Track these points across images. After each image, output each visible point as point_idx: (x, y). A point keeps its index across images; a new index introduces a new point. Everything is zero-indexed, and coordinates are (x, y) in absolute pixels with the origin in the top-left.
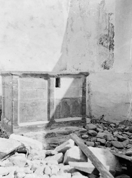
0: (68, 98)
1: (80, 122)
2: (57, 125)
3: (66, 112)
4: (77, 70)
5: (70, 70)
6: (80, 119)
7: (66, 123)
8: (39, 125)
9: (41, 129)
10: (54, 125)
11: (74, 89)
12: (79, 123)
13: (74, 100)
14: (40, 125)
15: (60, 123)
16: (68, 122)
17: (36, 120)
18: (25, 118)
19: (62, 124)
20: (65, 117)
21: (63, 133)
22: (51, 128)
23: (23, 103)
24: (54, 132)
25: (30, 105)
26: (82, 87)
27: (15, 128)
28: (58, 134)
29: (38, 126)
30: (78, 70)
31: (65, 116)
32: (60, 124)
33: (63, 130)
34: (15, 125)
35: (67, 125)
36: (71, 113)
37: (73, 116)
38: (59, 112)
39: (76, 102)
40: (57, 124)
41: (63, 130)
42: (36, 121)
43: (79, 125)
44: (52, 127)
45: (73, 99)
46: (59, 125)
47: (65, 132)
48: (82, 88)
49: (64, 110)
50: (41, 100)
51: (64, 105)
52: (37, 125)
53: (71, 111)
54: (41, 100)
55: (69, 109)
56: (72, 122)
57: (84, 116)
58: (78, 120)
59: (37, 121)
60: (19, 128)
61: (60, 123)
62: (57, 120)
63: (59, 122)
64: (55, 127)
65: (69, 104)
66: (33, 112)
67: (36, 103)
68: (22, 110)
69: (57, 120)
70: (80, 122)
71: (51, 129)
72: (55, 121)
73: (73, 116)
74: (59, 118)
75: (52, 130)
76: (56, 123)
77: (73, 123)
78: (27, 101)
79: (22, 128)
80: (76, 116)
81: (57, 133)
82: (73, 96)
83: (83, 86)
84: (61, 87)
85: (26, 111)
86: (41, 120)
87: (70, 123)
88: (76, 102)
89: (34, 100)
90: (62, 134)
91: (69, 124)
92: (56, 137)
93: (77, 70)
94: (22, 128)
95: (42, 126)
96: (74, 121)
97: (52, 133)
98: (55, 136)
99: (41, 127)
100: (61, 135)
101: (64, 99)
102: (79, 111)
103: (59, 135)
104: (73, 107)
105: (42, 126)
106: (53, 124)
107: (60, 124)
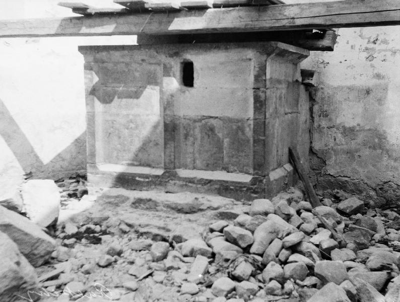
0: (217, 117)
1: (245, 189)
2: (182, 186)
3: (212, 155)
4: (374, 42)
5: (348, 43)
6: (246, 179)
7: (205, 184)
8: (141, 176)
9: (144, 186)
10: (175, 184)
11: (233, 92)
12: (241, 191)
13: (235, 127)
14: (143, 178)
15: (190, 182)
16: (210, 181)
17: (138, 163)
18: (115, 154)
19: (194, 185)
20: (208, 167)
21: (174, 206)
22: (167, 190)
23: (110, 118)
24: (153, 199)
25: (124, 125)
26: (254, 89)
27: (92, 173)
28: (164, 207)
29: (137, 179)
30: (378, 42)
31: (208, 165)
32: (190, 184)
33: (183, 198)
34: (91, 166)
35: (209, 190)
36: (226, 160)
37: (231, 168)
38: (193, 153)
39: (240, 133)
40: (181, 183)
41: (183, 198)
42: (137, 166)
43: (242, 198)
44: (170, 188)
45: (230, 120)
46: (186, 185)
47: (180, 204)
48: (252, 91)
49: (206, 148)
50: (148, 115)
51: (206, 137)
52: (135, 174)
53: (225, 152)
54: (148, 115)
55: (220, 148)
56: (221, 185)
57: (257, 174)
58: (239, 183)
59: (140, 165)
60: (97, 174)
61: (191, 181)
62: (183, 173)
63: (186, 178)
64: (175, 188)
65: (220, 135)
66: (131, 142)
67: (136, 122)
68: (108, 134)
69: (183, 173)
70: (245, 189)
71: (167, 192)
72: (176, 174)
73: (231, 168)
74: (191, 166)
75: (168, 194)
76: (180, 179)
77: (224, 189)
78: (118, 115)
79: (388, 206)
80: (241, 172)
81: (162, 202)
82: (230, 113)
83: (255, 84)
84: (195, 85)
85: (116, 138)
86: (149, 166)
87: (217, 186)
88: (240, 133)
89: (133, 115)
90: (173, 209)
91: (213, 187)
92: (157, 211)
93: (374, 42)
94: (104, 174)
95: (147, 180)
96: (227, 182)
97: (150, 200)
98: (155, 208)
99: (144, 182)
100: (169, 210)
101: (206, 120)
102: (247, 156)
103: (165, 209)
104: (232, 143)
105: (147, 180)
106: (172, 180)
107: (189, 183)
